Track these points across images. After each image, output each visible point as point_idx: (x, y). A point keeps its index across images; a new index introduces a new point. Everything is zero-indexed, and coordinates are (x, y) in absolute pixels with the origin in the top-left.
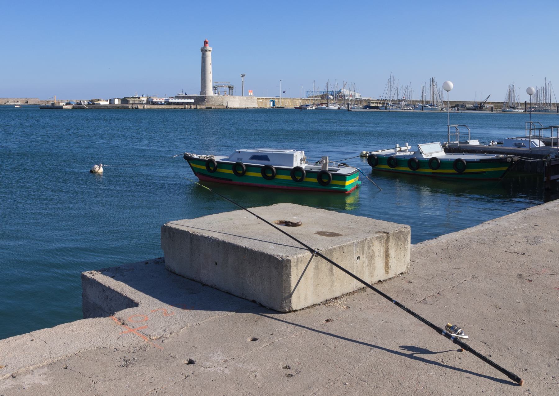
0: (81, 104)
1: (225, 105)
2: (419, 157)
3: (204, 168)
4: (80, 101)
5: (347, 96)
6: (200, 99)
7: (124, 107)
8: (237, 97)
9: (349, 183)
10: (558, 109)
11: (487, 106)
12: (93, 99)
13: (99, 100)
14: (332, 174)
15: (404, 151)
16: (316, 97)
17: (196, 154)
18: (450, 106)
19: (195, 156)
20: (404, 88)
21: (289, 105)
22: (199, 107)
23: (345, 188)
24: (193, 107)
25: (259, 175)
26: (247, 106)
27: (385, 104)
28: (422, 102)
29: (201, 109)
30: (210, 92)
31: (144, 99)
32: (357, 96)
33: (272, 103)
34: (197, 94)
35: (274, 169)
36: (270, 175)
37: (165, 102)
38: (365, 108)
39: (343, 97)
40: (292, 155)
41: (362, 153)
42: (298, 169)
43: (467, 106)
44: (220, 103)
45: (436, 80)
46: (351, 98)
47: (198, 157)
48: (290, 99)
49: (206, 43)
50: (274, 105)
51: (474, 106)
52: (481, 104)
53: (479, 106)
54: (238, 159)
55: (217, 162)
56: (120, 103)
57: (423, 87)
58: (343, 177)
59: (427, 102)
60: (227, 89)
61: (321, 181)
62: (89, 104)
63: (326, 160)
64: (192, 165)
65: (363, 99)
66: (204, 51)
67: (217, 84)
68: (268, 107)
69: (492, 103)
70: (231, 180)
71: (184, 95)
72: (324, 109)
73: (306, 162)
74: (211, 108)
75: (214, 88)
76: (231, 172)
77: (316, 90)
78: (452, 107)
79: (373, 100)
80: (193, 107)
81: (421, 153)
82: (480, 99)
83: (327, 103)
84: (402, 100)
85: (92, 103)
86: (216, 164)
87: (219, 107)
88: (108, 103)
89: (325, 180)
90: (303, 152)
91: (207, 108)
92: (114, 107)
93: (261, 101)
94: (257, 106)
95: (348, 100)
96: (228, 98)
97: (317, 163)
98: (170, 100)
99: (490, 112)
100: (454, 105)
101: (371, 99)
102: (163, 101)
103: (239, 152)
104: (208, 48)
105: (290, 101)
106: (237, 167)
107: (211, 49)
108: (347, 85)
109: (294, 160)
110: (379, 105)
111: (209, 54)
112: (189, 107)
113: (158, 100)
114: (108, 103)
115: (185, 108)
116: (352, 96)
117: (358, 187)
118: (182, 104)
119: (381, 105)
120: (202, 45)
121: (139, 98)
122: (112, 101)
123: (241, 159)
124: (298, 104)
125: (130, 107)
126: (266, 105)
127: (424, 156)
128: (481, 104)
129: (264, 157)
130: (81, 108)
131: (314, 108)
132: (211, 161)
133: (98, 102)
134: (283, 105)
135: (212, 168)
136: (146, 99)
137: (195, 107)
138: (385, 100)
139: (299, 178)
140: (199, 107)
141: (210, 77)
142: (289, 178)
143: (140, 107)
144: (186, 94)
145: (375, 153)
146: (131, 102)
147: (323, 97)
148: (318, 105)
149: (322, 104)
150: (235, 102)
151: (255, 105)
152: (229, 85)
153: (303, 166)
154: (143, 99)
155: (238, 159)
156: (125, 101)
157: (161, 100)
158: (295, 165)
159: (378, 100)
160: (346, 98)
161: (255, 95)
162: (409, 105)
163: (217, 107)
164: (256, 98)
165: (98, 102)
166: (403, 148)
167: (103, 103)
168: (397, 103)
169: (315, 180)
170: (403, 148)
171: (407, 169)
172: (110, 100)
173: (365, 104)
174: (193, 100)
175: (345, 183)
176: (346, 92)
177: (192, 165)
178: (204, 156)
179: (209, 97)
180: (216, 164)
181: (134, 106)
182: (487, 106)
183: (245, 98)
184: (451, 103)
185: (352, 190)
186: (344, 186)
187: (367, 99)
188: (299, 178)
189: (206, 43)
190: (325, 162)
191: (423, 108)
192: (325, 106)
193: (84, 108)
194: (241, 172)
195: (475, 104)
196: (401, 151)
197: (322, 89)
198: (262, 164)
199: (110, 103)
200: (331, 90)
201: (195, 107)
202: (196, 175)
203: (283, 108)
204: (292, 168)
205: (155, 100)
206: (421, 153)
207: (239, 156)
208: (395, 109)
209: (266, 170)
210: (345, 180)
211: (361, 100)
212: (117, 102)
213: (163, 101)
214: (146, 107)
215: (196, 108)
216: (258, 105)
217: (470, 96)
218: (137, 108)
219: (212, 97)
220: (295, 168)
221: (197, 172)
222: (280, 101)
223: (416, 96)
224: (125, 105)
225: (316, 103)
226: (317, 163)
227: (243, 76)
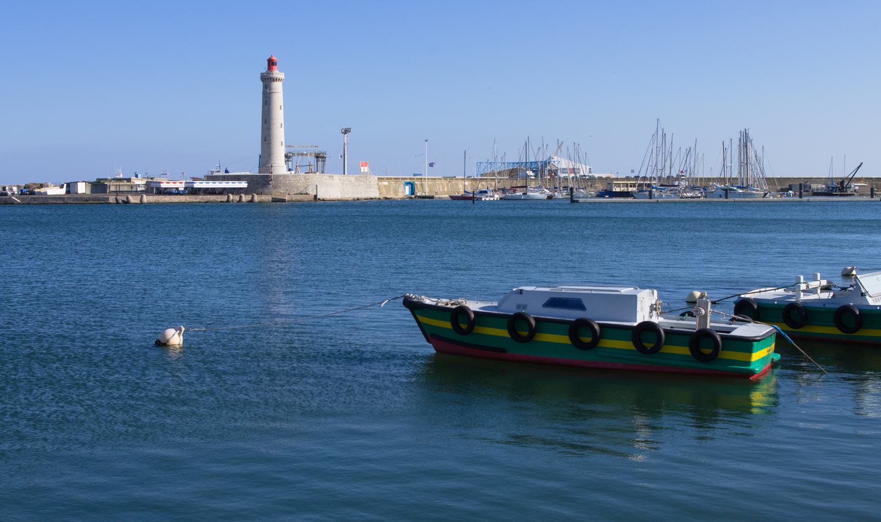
0: (6, 194)
1: (312, 193)
2: (859, 302)
3: (448, 325)
4: (4, 188)
5: (564, 170)
6: (261, 181)
7: (99, 199)
8: (336, 177)
9: (761, 356)
10: (876, 185)
11: (855, 186)
12: (28, 183)
13: (41, 186)
14: (722, 337)
15: (814, 291)
16: (499, 173)
17: (428, 296)
18: (779, 188)
19: (427, 301)
20: (683, 151)
21: (443, 191)
22: (257, 198)
23: (751, 367)
24: (245, 198)
25: (565, 339)
26: (356, 196)
27: (644, 186)
28: (722, 180)
29: (261, 203)
30: (280, 167)
31: (140, 182)
32: (584, 170)
33: (408, 188)
34: (253, 170)
35: (597, 327)
36: (588, 340)
37: (186, 188)
38: (601, 195)
39: (553, 173)
40: (634, 298)
41: (692, 295)
42: (648, 327)
43: (814, 186)
44: (302, 189)
45: (751, 135)
46: (572, 175)
47: (434, 303)
48: (445, 178)
49: (271, 63)
50: (413, 192)
51: (828, 187)
52: (842, 183)
53: (838, 188)
54: (519, 306)
55: (475, 312)
56: (89, 192)
57: (724, 149)
58: (747, 344)
59: (733, 181)
60: (312, 160)
61: (696, 353)
62: (22, 193)
63: (706, 309)
64: (421, 319)
65: (596, 176)
66: (267, 80)
67: (291, 150)
68: (400, 195)
69: (867, 179)
70: (503, 351)
71: (222, 173)
72: (518, 199)
73: (661, 314)
74: (284, 201)
75: (287, 157)
76: (504, 333)
77: (499, 160)
78: (782, 190)
79: (617, 179)
80: (245, 198)
81: (863, 295)
82: (840, 172)
83: (526, 187)
84: (678, 178)
85: (28, 191)
86: (473, 315)
87: (299, 197)
88: (63, 191)
89: (708, 351)
90: (655, 292)
91: (275, 200)
92: (77, 199)
93: (386, 183)
94: (378, 196)
95: (566, 179)
96: (316, 178)
97: (683, 315)
98: (197, 185)
99: (868, 198)
100: (786, 186)
101: (613, 176)
102: (181, 187)
103: (521, 292)
104: (277, 73)
105: (444, 182)
106: (516, 322)
107: (281, 75)
108: (564, 148)
109: (639, 309)
110: (630, 189)
111: (278, 87)
112: (237, 198)
113: (171, 185)
114: (63, 191)
115: (228, 201)
116: (573, 170)
117: (774, 365)
118: (222, 192)
119: (634, 189)
120: (264, 68)
121: (129, 180)
122: (71, 187)
123: (525, 307)
124: (461, 188)
125: (112, 199)
126: (396, 192)
127: (871, 302)
128: (842, 183)
129: (575, 303)
130: (6, 203)
131: (497, 196)
132: (462, 311)
133: (42, 190)
134: (430, 191)
135: (464, 326)
136: (144, 182)
137: (249, 198)
138: (644, 178)
139: (649, 346)
140: (257, 198)
141: (279, 134)
142: (628, 345)
143: (133, 199)
144: (227, 171)
145: (747, 296)
146: (113, 189)
147: (513, 173)
148: (504, 190)
149: (514, 189)
150: (333, 187)
151: (375, 194)
152: (317, 151)
153: (656, 319)
154: (137, 182)
155: (519, 306)
156: (98, 186)
157: (177, 185)
158: (640, 320)
159: (628, 178)
160: (562, 175)
161: (373, 172)
162: (693, 188)
163: (295, 198)
164: (376, 177)
165: (42, 190)
166: (813, 284)
167: (54, 191)
168: (668, 183)
169: (685, 351)
170: (813, 284)
171: (833, 331)
172: (68, 185)
173: (600, 187)
174: (244, 185)
175: (750, 356)
176: (562, 163)
177: (421, 319)
178: (444, 300)
179: (278, 176)
180: (473, 315)
181: (121, 198)
182: (855, 186)
183: (352, 178)
184: (781, 180)
185: (764, 373)
186: (748, 363)
187: (604, 176)
188: (649, 346)
189: (271, 63)
190: (703, 312)
191: (727, 192)
192: (519, 193)
193: (12, 203)
194: (525, 334)
195: (829, 183)
196: (808, 291)
197: (514, 157)
198: (572, 315)
199: (68, 192)
200: (532, 159)
201: (249, 198)
202: (428, 341)
203: (432, 197)
204: (635, 324)
205: (164, 185)
206: (863, 295)
207: (521, 300)
208: (666, 196)
209: (579, 329)
210: (750, 351)
211: (592, 179)
212: (82, 188)
213: (181, 187)
214: (146, 199)
215: (252, 201)
216: (381, 193)
217: (819, 167)
218: (127, 202)
219: (285, 176)
220: (640, 325)
221: (431, 335)
222: (426, 184)
223: (709, 167)
224: (100, 195)
225: (499, 186)
226: (683, 315)
227: (346, 131)
